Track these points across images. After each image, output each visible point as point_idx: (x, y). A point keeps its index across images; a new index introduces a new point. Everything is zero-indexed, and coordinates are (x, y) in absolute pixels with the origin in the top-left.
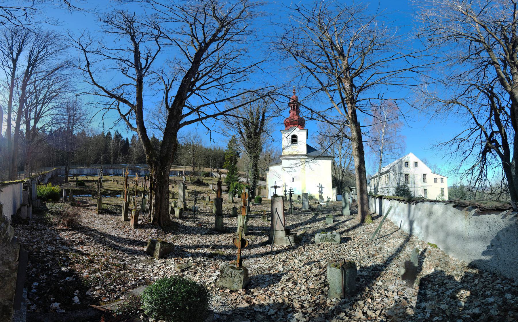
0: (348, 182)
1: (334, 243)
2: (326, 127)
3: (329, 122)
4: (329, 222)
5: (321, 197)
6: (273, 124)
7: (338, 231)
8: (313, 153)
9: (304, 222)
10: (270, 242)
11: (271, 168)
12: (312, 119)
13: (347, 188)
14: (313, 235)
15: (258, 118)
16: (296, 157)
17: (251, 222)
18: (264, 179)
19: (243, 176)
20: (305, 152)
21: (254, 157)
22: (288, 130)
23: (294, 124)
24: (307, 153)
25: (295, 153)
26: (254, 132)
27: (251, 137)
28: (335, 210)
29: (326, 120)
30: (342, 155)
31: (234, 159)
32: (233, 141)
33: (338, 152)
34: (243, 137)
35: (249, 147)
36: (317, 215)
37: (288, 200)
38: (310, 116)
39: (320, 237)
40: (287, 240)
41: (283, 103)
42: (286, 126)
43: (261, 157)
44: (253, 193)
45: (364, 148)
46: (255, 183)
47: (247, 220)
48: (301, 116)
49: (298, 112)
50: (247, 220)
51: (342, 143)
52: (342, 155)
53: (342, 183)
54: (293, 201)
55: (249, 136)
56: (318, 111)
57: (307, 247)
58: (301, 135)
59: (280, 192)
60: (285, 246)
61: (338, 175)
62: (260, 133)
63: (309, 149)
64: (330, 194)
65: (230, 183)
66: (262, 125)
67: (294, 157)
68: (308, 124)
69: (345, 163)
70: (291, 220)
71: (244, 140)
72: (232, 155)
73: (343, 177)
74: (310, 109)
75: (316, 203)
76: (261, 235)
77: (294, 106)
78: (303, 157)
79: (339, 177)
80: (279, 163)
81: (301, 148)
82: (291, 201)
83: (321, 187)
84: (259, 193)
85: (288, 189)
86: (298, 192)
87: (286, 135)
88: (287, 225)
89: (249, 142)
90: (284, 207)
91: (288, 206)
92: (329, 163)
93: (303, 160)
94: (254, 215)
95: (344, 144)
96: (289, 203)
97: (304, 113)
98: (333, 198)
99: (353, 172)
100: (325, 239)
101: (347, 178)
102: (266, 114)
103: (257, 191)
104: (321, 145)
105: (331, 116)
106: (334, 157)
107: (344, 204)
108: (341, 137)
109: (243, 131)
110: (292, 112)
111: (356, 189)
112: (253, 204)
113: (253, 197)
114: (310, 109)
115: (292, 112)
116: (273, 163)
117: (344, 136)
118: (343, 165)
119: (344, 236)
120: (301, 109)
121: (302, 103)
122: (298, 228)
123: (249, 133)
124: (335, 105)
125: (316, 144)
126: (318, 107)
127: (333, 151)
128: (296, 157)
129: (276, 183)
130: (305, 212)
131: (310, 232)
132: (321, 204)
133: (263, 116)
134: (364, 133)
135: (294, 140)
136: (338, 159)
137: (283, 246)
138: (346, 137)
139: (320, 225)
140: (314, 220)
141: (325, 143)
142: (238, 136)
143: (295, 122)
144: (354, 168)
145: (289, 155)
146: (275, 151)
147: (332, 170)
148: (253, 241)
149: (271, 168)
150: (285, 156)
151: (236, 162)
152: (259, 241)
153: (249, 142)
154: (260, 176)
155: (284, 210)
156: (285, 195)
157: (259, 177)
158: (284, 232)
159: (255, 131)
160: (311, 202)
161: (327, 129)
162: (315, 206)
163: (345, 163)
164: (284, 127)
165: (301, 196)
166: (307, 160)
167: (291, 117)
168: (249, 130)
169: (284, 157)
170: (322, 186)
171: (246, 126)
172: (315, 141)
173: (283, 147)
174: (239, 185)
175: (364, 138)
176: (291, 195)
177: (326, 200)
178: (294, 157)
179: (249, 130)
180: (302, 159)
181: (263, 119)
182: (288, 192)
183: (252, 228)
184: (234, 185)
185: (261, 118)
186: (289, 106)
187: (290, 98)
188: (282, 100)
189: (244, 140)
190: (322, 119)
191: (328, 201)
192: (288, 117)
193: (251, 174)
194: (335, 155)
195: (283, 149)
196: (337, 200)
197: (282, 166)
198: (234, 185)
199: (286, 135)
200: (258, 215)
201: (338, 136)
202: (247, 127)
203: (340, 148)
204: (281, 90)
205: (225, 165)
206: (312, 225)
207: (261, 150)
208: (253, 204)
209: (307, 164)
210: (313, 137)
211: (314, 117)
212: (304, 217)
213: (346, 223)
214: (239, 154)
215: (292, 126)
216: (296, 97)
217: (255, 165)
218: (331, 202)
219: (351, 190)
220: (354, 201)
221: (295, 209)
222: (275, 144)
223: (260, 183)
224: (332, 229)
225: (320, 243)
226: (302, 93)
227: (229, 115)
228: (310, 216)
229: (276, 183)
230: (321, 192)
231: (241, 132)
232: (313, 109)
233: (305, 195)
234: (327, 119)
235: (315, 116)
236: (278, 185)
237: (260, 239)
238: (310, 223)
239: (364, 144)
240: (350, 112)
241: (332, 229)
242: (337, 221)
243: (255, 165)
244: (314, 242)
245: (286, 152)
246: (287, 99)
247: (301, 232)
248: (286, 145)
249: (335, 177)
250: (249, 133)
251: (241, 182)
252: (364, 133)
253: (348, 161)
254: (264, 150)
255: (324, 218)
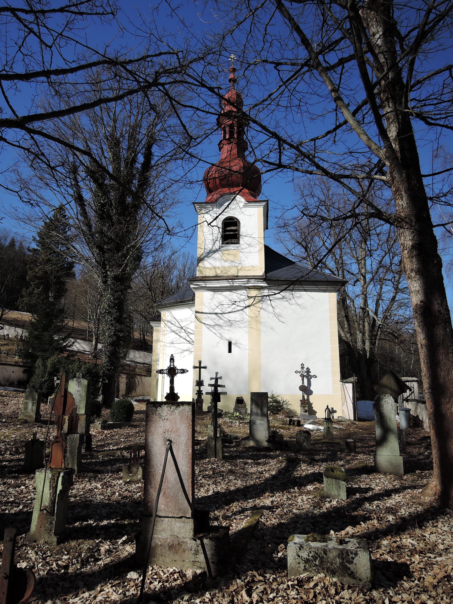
0: (392, 360)
1: (352, 581)
2: (318, 192)
3: (325, 172)
4: (334, 492)
5: (306, 404)
6: (176, 182)
7: (363, 527)
8: (281, 273)
9: (254, 486)
10: (141, 561)
11: (166, 314)
12: (280, 166)
13: (387, 380)
14: (282, 534)
15: (134, 161)
16: (237, 283)
17: (80, 488)
18: (146, 346)
19: (83, 335)
20: (261, 271)
21: (116, 278)
22: (213, 203)
23: (231, 185)
24: (267, 271)
25: (233, 272)
26: (122, 203)
27: (110, 217)
28: (351, 449)
29: (318, 167)
30: (369, 277)
31: (57, 277)
32: (56, 224)
33: (354, 268)
34: (84, 213)
35: (100, 248)
36: (293, 463)
37: (205, 408)
38: (274, 158)
39: (304, 554)
40: (197, 552)
41: (199, 112)
42: (210, 191)
43: (137, 281)
44: (110, 391)
45: (440, 246)
46: (115, 357)
47: (68, 483)
48: (251, 160)
49: (242, 147)
50: (68, 483)
51: (366, 235)
52: (369, 277)
53: (371, 361)
54: (220, 415)
55: (103, 215)
56: (295, 140)
57: (261, 587)
58: (249, 216)
59: (186, 391)
60: (189, 574)
61: (359, 336)
62: (137, 207)
63: (272, 259)
64: (334, 397)
65: (34, 358)
66: (145, 183)
67: (230, 282)
68: (271, 183)
69: (379, 297)
70: (216, 475)
71: (89, 226)
72: (48, 268)
73: (373, 344)
74: (275, 135)
75: (291, 422)
76: (111, 534)
77: (231, 126)
78: (252, 283)
79: (363, 343)
80: (187, 300)
81: (250, 257)
82: (216, 414)
83: (307, 375)
84: (130, 388)
85: (206, 377)
86: (237, 387)
87: (209, 218)
88: (201, 493)
89: (101, 232)
90: (194, 431)
91: (206, 432)
92: (327, 301)
93: (254, 293)
94: (103, 463)
95: (373, 242)
96: (208, 420)
97: (261, 147)
98: (345, 410)
99: (408, 328)
100: (319, 561)
101: (387, 345)
102: (155, 149)
103: (123, 381)
104: (306, 248)
105: (331, 155)
106: (344, 283)
107: (378, 432)
108: (362, 217)
109: (87, 196)
110: (226, 147)
111: (420, 383)
112: (105, 426)
113: (107, 403)
114: (275, 135)
115: (226, 147)
116: (171, 299)
117: (372, 215)
118: (371, 306)
119: (384, 549)
120: (253, 135)
121: (252, 115)
122: (235, 506)
123: (103, 205)
124: (347, 115)
125: (291, 244)
126: (298, 129)
127: (341, 265)
128: (237, 283)
129: (172, 359)
130: (259, 453)
131: (271, 520)
132: (308, 426)
133: (148, 156)
134: (436, 198)
135: (231, 232)
136: (358, 289)
137: (182, 575)
138: (379, 214)
139: (302, 501)
140: (285, 482)
141: (318, 242)
142: (72, 210)
143: (234, 178)
144: (409, 312)
145: (217, 278)
146: (180, 267)
147: (340, 324)
148: (84, 563)
149: (166, 314)
150: (205, 279)
151: (61, 291)
152: (104, 561)
153: (101, 232)
154: (137, 335)
155: (195, 443)
156: (199, 393)
157: (130, 334)
158: (189, 525)
159: (121, 201)
160: (277, 421)
161: (323, 198)
162: (288, 433)
163: (379, 297)
164: (203, 195)
165: (247, 400)
166: (266, 292)
167: (221, 162)
168: (106, 193)
169: (202, 284)
170: (308, 371)
171: (96, 181)
172: (286, 236)
173: (200, 252)
174: (70, 364)
175: (437, 213)
176: (216, 396)
177: (321, 414)
178: (230, 282)
179: (106, 193)
180: (249, 288)
181: (147, 166)
182: (206, 389)
183: (88, 507)
184: (49, 363)
185: (141, 159)
186: (219, 124)
187: (221, 97)
188: (201, 105)
189: (89, 226)
190: (306, 165)
191: (328, 420)
192: (215, 161)
193: (107, 330)
194: (348, 276)
195: (200, 260)
196: (358, 417)
197: (194, 309)
198: (49, 363)
199: (209, 218)
200: (117, 460)
201: (355, 216)
202: (100, 186)
203: (361, 253)
204: (198, 67)
205: (26, 299)
206: (278, 497)
207: (139, 258)
208: (105, 426)
209: (266, 304)
210: (281, 222)
211: (285, 160)
212: (254, 470)
213: (390, 502)
214: (71, 265)
215: (226, 190)
216: (238, 96)
217: (119, 305)
218: (339, 422)
219: (403, 387)
220: (414, 422)
221: (227, 440)
222: (175, 242)
223: (135, 356)
224: (340, 518)
225: (304, 575)
226: (253, 79)
227: (40, 133)
228: (271, 467)
229: (172, 359)
230: (306, 390)
231: (80, 199)
232: (282, 134)
233: (260, 399)
234: (321, 164)
235: (288, 156)
236: (178, 365)
237: (109, 552)
238: (273, 492)
239: (438, 232)
240: (392, 133)
241: (340, 518)
242: (360, 490)
243: (119, 305)
244: (282, 565)
245: (208, 267)
246: (215, 100)
247: (243, 524)
248: (209, 246)
249: (347, 343)
250: (103, 205)
251: (74, 353)
252: (436, 198)
253: (388, 291)
254: (148, 261)
255: (317, 478)
